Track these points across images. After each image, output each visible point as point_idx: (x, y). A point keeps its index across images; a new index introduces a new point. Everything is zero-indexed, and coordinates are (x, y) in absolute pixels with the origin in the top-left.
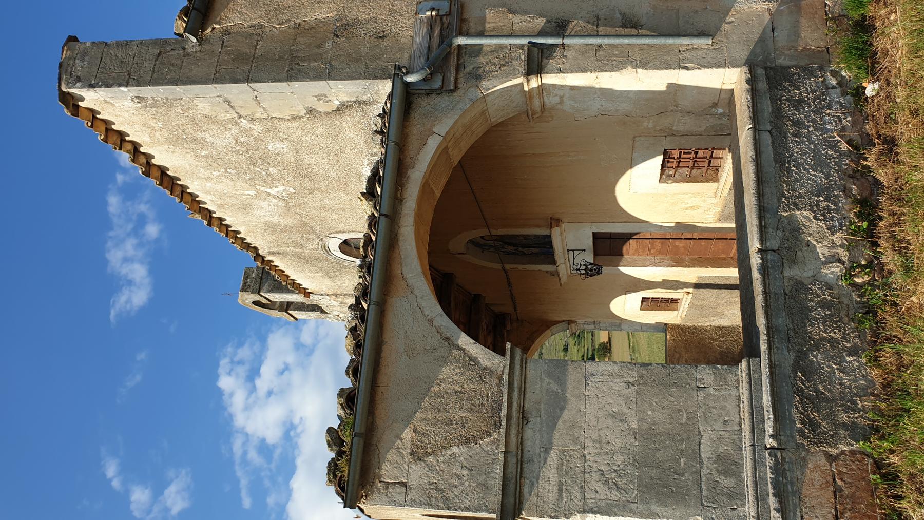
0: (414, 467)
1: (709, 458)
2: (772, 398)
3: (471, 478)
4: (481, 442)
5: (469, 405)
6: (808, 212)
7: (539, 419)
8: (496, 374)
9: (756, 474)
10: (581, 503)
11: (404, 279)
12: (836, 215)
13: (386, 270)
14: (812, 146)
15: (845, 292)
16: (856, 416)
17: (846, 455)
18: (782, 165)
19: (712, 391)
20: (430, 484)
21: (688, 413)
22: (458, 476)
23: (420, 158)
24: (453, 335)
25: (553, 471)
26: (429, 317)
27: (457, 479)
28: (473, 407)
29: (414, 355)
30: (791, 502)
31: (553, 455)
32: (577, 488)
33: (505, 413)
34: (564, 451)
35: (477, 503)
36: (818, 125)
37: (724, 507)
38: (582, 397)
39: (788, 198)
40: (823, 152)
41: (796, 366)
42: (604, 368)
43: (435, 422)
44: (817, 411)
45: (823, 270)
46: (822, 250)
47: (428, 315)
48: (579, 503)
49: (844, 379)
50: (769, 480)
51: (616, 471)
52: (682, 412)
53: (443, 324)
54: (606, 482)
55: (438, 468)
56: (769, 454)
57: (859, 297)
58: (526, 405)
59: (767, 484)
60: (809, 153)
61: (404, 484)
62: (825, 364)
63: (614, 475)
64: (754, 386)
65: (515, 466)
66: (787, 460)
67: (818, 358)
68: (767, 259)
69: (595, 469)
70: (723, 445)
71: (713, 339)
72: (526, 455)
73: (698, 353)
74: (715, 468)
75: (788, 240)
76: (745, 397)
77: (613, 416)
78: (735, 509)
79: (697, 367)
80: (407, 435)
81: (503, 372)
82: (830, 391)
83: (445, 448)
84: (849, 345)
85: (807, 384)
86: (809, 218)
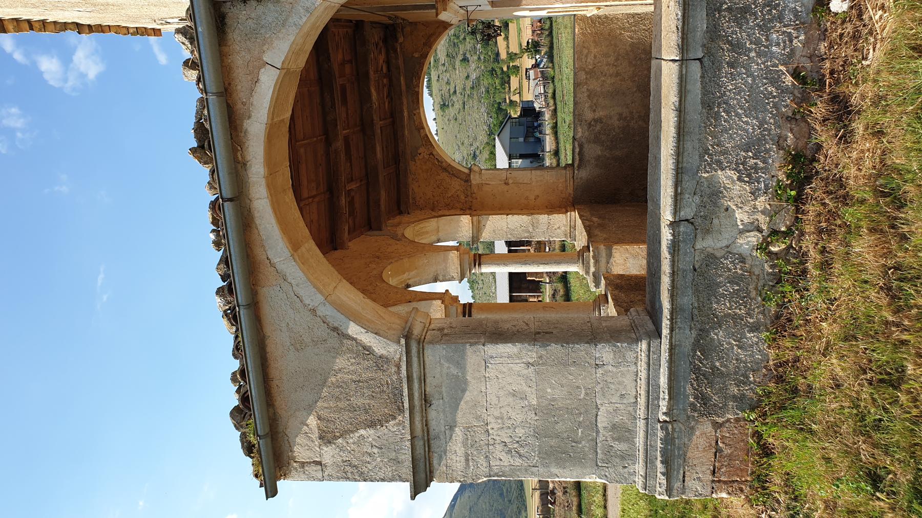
0: (325, 449)
1: (605, 428)
2: (669, 381)
3: (382, 455)
4: (387, 425)
5: (370, 393)
6: (732, 172)
7: (441, 401)
8: (393, 362)
9: (647, 442)
10: (487, 470)
11: (272, 265)
12: (763, 175)
13: (248, 256)
14: (750, 80)
15: (758, 263)
16: (746, 388)
17: (731, 423)
18: (710, 108)
19: (610, 368)
20: (344, 461)
21: (586, 389)
22: (370, 454)
23: (255, 103)
24: (341, 324)
25: (459, 445)
26: (310, 306)
27: (369, 457)
28: (374, 394)
29: (303, 347)
30: (676, 463)
31: (458, 432)
32: (482, 457)
33: (408, 406)
34: (469, 427)
35: (390, 475)
36: (762, 48)
37: (617, 466)
38: (483, 379)
39: (711, 155)
40: (761, 89)
41: (696, 345)
42: (503, 351)
43: (339, 410)
44: (711, 387)
45: (738, 241)
46: (741, 217)
47: (309, 305)
48: (485, 470)
49: (741, 355)
50: (659, 448)
51: (518, 442)
52: (581, 389)
53: (328, 313)
54: (510, 451)
55: (349, 448)
56: (661, 428)
57: (771, 268)
58: (428, 389)
59: (657, 450)
60: (744, 91)
61: (319, 463)
62: (725, 341)
63: (516, 445)
64: (652, 366)
65: (423, 447)
66: (677, 430)
67: (718, 335)
68: (679, 232)
69: (498, 442)
70: (618, 416)
71: (624, 29)
72: (432, 433)
73: (607, 46)
74: (610, 435)
75: (705, 207)
76: (643, 375)
77: (514, 394)
78: (625, 467)
79: (596, 345)
80: (312, 421)
81: (400, 359)
82: (726, 366)
83: (352, 432)
84: (751, 321)
85: (705, 362)
86: (732, 178)
